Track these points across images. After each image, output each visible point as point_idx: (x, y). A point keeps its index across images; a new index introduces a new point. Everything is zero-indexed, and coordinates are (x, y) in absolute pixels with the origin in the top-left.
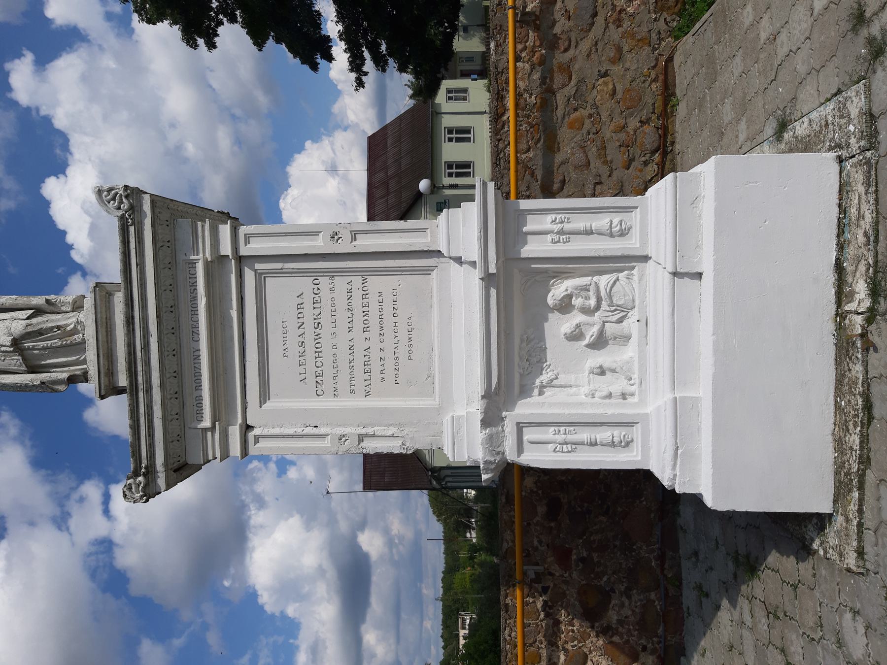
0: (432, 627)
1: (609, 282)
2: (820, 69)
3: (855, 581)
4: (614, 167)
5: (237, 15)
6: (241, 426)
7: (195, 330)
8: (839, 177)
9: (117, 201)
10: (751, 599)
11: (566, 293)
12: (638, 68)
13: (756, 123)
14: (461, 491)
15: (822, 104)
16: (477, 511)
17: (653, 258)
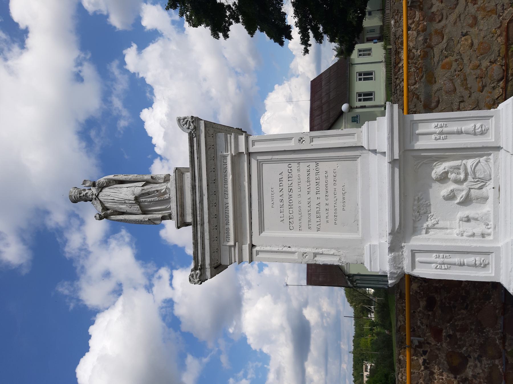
0: (347, 369)
1: (473, 164)
4: (472, 91)
5: (240, 18)
6: (249, 245)
11: (444, 171)
12: (488, 29)
14: (365, 289)
16: (375, 301)
17: (504, 148)
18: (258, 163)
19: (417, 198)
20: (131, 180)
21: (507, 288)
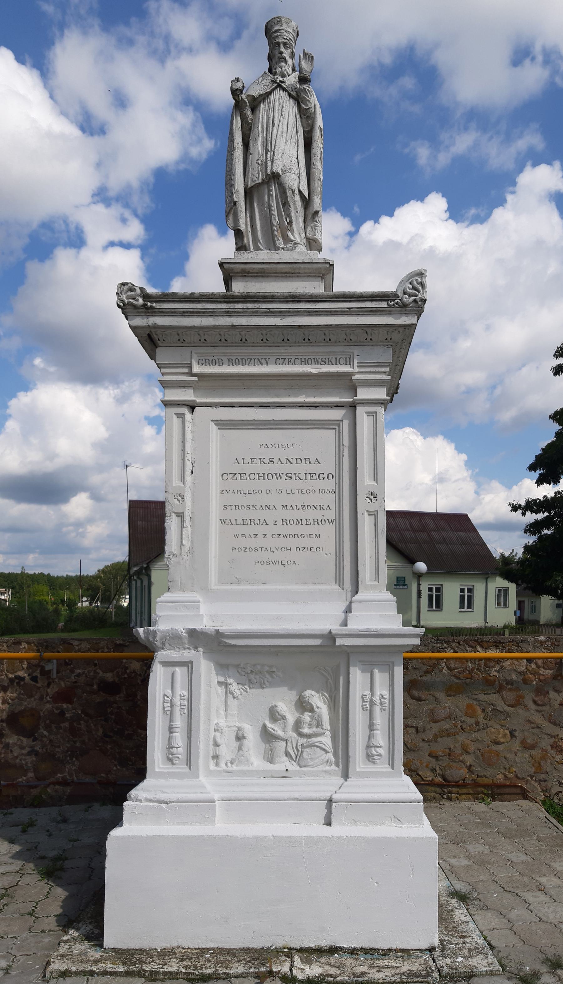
1: (324, 745)
2: (513, 931)
3: (37, 969)
4: (431, 744)
6: (194, 401)
7: (287, 361)
8: (416, 949)
9: (411, 291)
10: (21, 873)
11: (315, 707)
13: (466, 874)
14: (127, 594)
15: (482, 933)
16: (109, 607)
17: (346, 783)
18: (338, 422)
19: (274, 670)
20: (312, 166)
21: (138, 787)
